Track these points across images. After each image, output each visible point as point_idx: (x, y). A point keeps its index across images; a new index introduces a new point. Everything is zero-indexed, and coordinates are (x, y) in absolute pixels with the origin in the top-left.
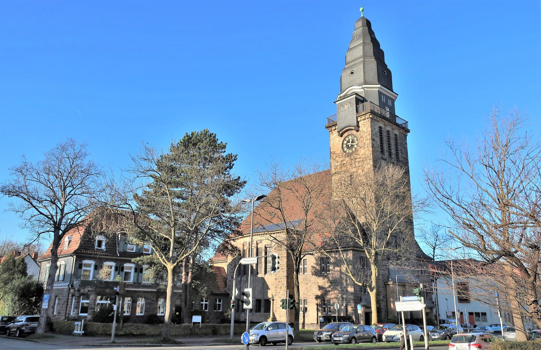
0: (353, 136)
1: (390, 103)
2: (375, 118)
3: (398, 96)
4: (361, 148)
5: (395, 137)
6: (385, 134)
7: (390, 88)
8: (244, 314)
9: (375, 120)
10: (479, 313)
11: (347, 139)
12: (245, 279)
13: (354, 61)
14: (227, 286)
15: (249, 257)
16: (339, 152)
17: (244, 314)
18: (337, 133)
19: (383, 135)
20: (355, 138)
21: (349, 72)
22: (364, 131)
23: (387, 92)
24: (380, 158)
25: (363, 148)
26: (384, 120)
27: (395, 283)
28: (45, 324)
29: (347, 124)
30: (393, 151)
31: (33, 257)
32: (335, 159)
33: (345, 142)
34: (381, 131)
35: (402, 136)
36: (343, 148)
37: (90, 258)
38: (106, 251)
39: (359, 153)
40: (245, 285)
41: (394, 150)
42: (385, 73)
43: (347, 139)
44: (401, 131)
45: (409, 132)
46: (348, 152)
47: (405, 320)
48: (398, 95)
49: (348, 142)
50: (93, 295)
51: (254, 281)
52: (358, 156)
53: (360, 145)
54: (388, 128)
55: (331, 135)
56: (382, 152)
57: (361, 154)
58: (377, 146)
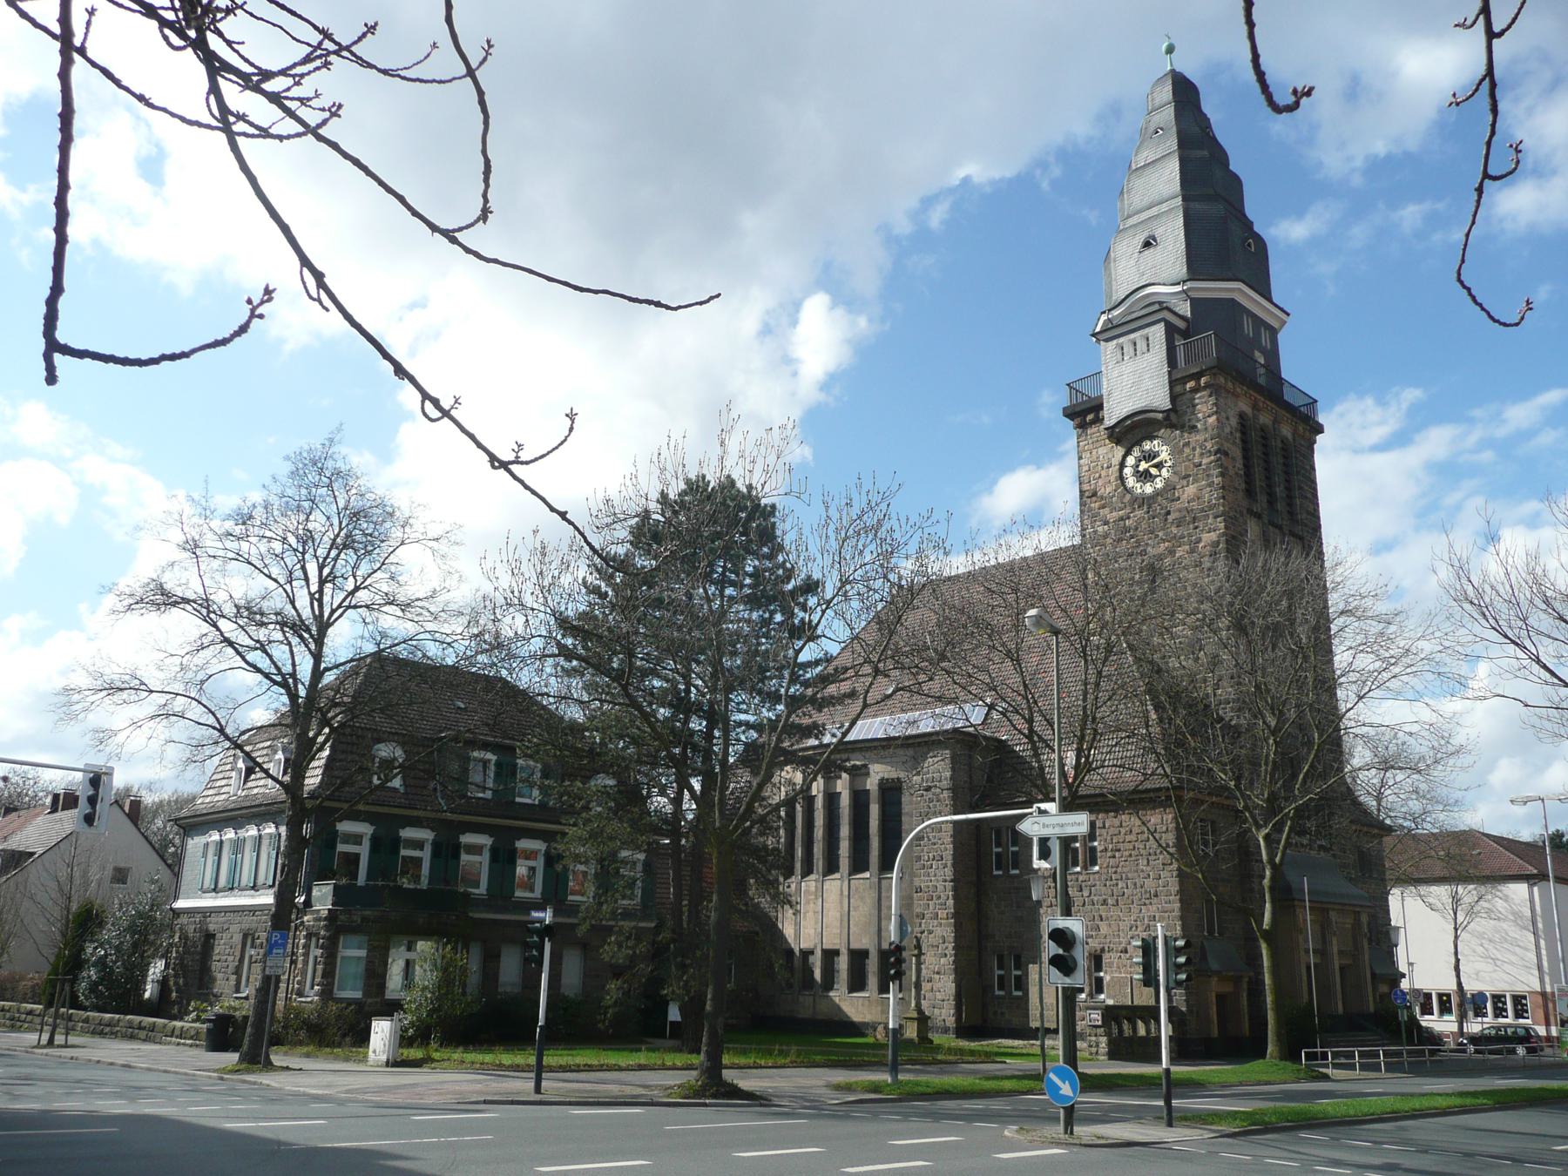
1: (1265, 339)
8: (811, 999)
9: (1229, 392)
10: (1428, 996)
12: (813, 889)
13: (1149, 208)
17: (811, 999)
21: (1141, 238)
24: (1245, 512)
26: (1251, 392)
30: (1278, 490)
31: (127, 811)
37: (355, 816)
38: (406, 793)
40: (812, 905)
41: (1282, 488)
42: (1249, 245)
45: (1322, 432)
47: (1284, 1021)
48: (1288, 314)
52: (1177, 505)
56: (1250, 493)
57: (1185, 497)
58: (1236, 473)
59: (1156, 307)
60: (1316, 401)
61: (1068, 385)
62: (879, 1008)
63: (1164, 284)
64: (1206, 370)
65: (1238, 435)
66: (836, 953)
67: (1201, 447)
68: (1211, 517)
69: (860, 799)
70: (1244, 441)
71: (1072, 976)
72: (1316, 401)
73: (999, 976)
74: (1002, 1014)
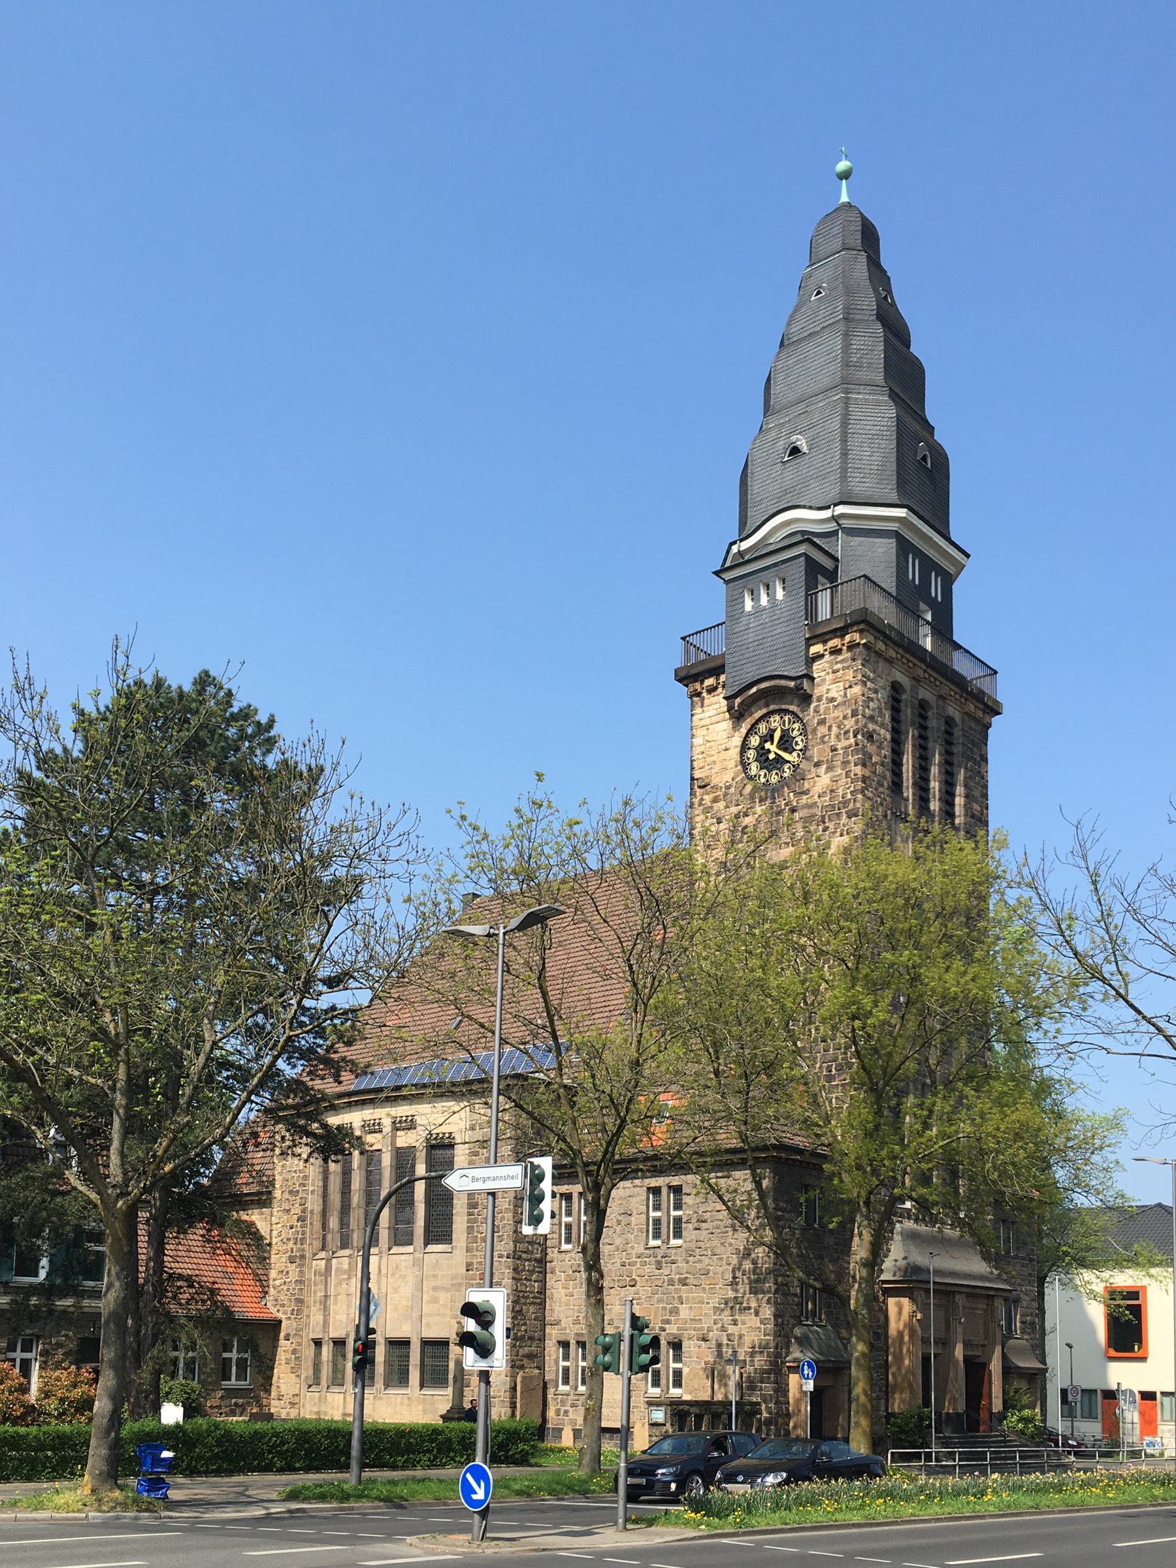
0: (786, 718)
1: (936, 590)
2: (880, 646)
3: (969, 564)
4: (817, 765)
5: (947, 732)
6: (912, 712)
7: (941, 524)
11: (763, 728)
12: (346, 1266)
14: (272, 1291)
15: (496, 1162)
16: (727, 777)
18: (725, 702)
19: (903, 717)
20: (796, 726)
22: (833, 700)
23: (929, 540)
25: (824, 767)
27: (937, 1287)
28: (304, 1427)
29: (768, 671)
32: (711, 807)
33: (755, 741)
34: (899, 701)
35: (971, 728)
36: (745, 765)
39: (806, 786)
40: (344, 1286)
43: (763, 728)
44: (971, 707)
46: (763, 780)
48: (968, 556)
49: (770, 737)
50: (521, 1228)
51: (384, 1271)
52: (804, 799)
53: (815, 753)
54: (924, 694)
55: (698, 710)
59: (799, 538)
60: (996, 672)
61: (683, 639)
62: (421, 1407)
63: (810, 508)
64: (851, 625)
65: (887, 714)
66: (405, 1343)
67: (839, 727)
68: (845, 816)
69: (404, 1158)
70: (895, 719)
71: (489, 1359)
72: (996, 672)
73: (563, 1367)
74: (566, 1412)
